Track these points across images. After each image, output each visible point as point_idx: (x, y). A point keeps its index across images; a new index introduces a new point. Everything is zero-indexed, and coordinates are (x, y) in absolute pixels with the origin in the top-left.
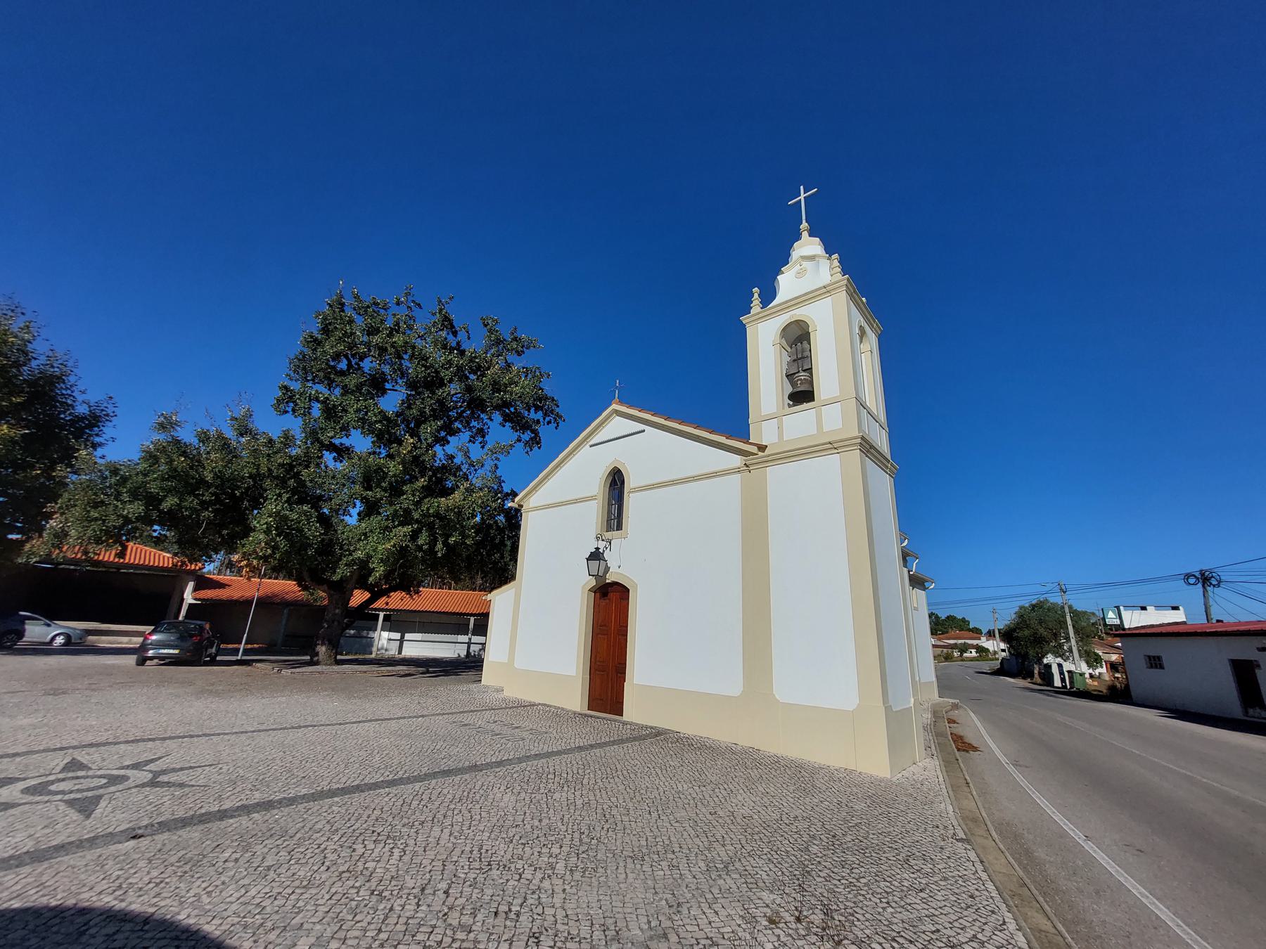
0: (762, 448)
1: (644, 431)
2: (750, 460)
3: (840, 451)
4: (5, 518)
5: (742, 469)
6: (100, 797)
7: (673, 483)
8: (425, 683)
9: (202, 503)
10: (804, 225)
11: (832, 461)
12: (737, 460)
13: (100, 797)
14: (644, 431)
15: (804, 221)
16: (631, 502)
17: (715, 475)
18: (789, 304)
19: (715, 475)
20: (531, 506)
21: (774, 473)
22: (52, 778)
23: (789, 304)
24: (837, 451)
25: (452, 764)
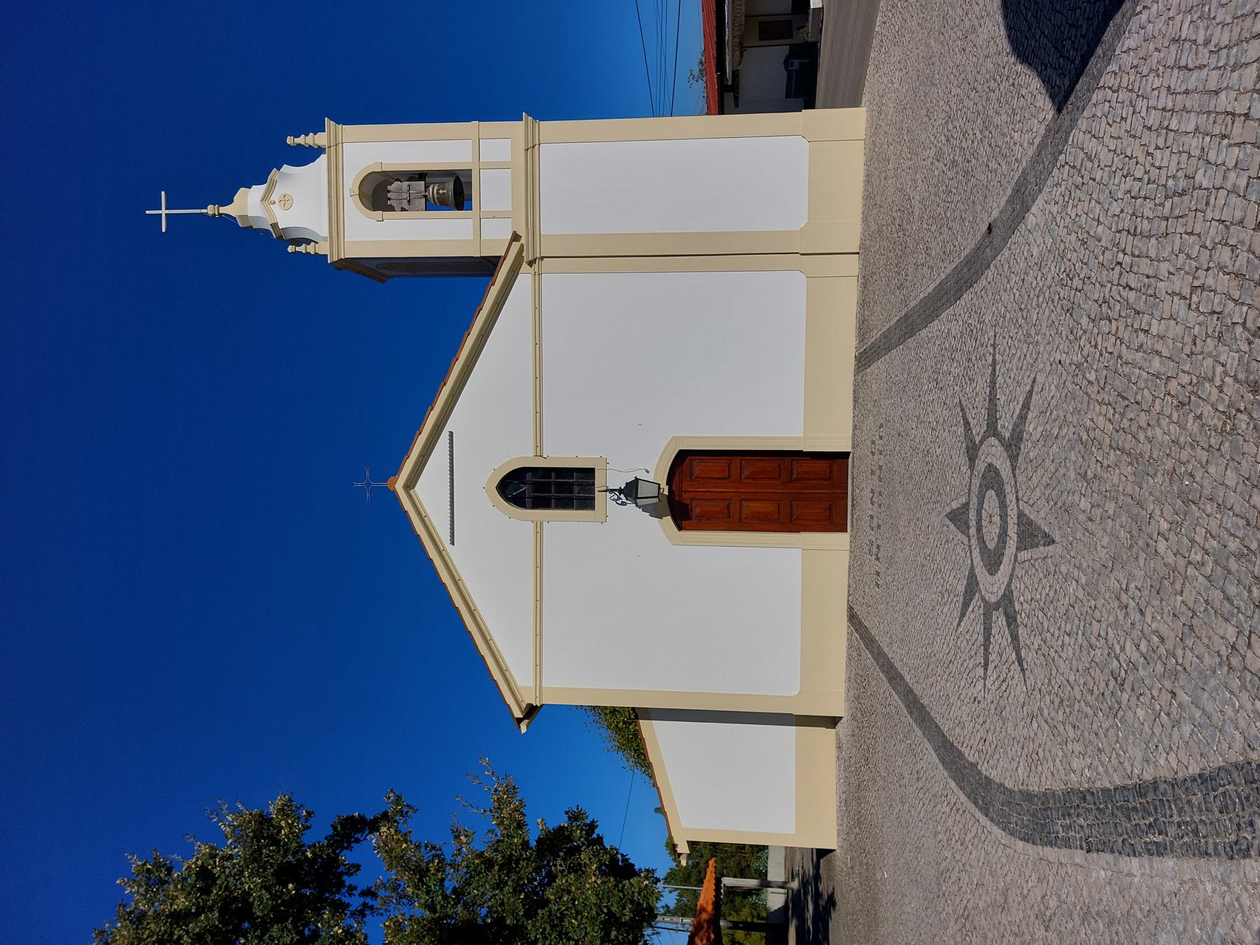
0: (516, 237)
1: (451, 433)
2: (527, 256)
3: (537, 143)
4: (295, 894)
5: (536, 270)
6: (1021, 515)
7: (539, 413)
8: (743, 60)
9: (393, 835)
10: (210, 210)
11: (546, 152)
12: (524, 280)
13: (1021, 515)
14: (451, 433)
15: (204, 211)
16: (559, 454)
17: (537, 308)
18: (333, 195)
19: (537, 308)
20: (531, 684)
21: (550, 226)
22: (1011, 498)
23: (333, 195)
24: (537, 146)
25: (938, 713)
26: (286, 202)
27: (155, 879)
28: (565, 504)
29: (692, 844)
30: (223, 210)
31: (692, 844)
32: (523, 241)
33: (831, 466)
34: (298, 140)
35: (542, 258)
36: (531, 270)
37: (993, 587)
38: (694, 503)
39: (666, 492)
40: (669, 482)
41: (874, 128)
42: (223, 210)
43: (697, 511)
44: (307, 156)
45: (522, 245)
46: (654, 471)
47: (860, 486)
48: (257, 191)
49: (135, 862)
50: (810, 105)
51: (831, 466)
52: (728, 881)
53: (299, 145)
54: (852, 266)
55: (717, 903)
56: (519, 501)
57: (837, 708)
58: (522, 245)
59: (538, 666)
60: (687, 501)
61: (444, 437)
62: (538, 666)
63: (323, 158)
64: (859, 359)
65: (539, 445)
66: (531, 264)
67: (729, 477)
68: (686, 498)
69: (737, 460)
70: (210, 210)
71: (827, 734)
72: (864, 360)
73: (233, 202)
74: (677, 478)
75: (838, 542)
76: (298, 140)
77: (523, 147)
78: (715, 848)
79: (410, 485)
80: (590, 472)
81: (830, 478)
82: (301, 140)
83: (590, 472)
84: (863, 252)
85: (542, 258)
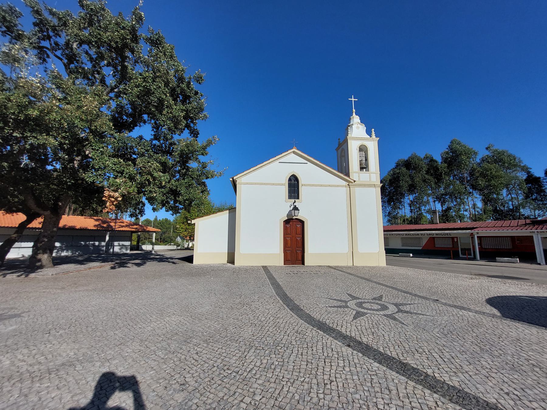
0: (355, 181)
1: (307, 163)
6: (366, 314)
10: (354, 110)
12: (345, 183)
13: (366, 314)
14: (307, 163)
16: (303, 191)
19: (338, 186)
26: (358, 128)
27: (199, 80)
28: (290, 192)
29: (194, 224)
30: (354, 113)
31: (194, 224)
32: (354, 183)
33: (300, 260)
34: (373, 132)
35: (350, 188)
36: (347, 185)
37: (392, 309)
38: (290, 225)
39: (293, 218)
40: (296, 219)
41: (383, 268)
42: (354, 113)
43: (288, 226)
44: (369, 133)
45: (353, 183)
46: (301, 215)
47: (298, 268)
48: (359, 121)
49: (204, 75)
50: (386, 253)
51: (300, 260)
52: (154, 234)
53: (372, 132)
54: (350, 264)
55: (149, 231)
56: (290, 180)
57: (239, 262)
58: (353, 183)
59: (247, 184)
60: (290, 223)
61: (306, 162)
62: (247, 184)
63: (369, 137)
64: (266, 267)
65: (305, 185)
66: (348, 185)
67: (297, 234)
68: (291, 223)
69: (301, 236)
70: (354, 110)
71: (224, 260)
72: (265, 268)
73: (356, 115)
74: (296, 221)
75: (281, 263)
76: (373, 132)
77: (375, 184)
78: (193, 229)
79: (294, 152)
80: (298, 198)
81: (297, 260)
82: (373, 132)
83: (298, 198)
84: (353, 267)
85: (350, 188)
